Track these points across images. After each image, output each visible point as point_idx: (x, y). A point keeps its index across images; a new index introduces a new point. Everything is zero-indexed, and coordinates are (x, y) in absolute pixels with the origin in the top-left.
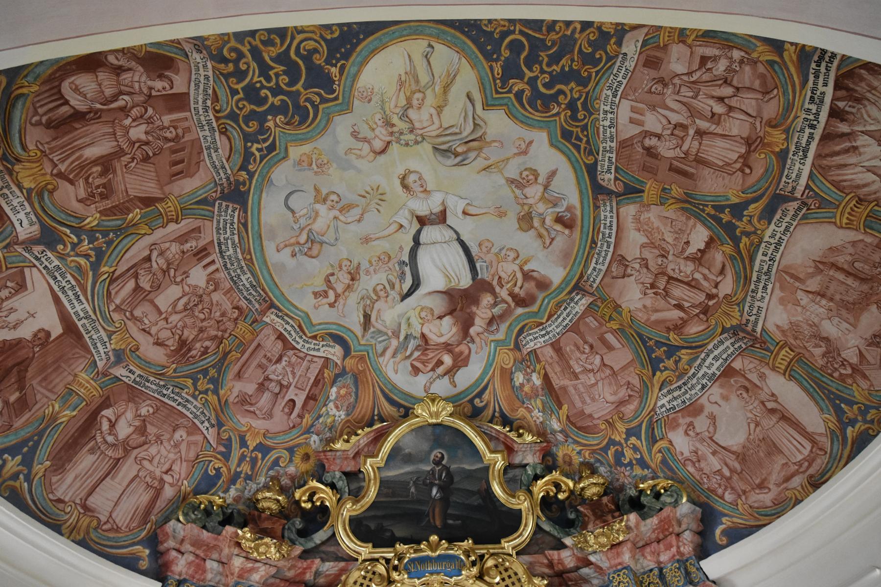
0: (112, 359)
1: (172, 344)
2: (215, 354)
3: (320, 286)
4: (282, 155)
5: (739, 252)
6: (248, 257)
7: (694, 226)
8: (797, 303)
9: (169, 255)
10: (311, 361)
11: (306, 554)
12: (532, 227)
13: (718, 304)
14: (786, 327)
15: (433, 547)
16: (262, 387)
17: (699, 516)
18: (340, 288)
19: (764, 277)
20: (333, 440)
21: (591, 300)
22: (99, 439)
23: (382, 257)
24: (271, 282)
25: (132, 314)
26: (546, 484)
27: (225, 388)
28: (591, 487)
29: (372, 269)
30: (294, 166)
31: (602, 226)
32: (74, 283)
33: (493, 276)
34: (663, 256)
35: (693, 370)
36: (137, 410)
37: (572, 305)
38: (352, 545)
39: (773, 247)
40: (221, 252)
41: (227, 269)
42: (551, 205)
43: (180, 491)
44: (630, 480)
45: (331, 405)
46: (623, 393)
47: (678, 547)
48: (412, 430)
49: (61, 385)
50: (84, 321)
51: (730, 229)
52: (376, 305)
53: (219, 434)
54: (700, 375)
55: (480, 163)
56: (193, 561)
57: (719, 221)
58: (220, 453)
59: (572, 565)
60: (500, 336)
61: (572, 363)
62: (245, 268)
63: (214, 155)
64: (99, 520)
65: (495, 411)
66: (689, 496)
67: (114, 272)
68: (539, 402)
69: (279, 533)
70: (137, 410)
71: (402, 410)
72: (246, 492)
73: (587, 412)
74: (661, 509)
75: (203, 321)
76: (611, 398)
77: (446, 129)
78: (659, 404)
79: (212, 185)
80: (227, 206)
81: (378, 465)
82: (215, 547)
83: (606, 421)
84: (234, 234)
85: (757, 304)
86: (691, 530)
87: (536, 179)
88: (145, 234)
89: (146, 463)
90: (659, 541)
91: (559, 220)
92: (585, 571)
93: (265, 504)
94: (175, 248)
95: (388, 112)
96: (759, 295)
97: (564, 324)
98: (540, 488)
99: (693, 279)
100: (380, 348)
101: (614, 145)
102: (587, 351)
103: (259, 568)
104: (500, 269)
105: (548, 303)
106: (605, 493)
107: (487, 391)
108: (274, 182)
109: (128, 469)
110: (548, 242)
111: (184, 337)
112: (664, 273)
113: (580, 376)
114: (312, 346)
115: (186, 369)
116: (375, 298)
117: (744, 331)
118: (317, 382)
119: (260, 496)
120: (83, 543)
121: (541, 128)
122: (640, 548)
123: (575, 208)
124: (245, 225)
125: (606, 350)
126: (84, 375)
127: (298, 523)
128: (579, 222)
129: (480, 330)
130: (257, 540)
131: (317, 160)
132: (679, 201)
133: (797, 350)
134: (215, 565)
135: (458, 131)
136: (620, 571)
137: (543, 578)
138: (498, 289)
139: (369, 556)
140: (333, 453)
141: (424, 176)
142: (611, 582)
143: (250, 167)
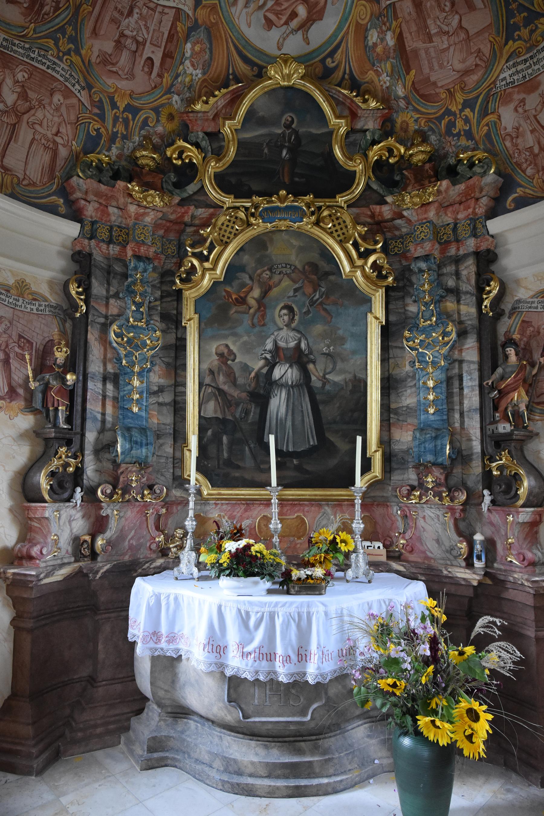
2: (67, 8)
10: (162, 13)
11: (183, 202)
15: (282, 200)
16: (119, 45)
17: (500, 185)
20: (192, 101)
26: (381, 149)
27: (86, 47)
36: (14, 77)
43: (72, 150)
44: (454, 149)
45: (187, 63)
46: (471, 61)
47: (474, 209)
48: (266, 93)
53: (90, 96)
56: (98, 208)
58: (96, 115)
59: (389, 217)
61: (429, 22)
64: (18, 178)
65: (345, 73)
66: (496, 168)
68: (388, 65)
69: (159, 185)
70: (14, 77)
71: (255, 68)
72: (125, 150)
73: (432, 79)
74: (471, 177)
76: (459, 66)
81: (236, 127)
82: (113, 197)
86: (489, 196)
89: (37, 127)
90: (460, 203)
92: (399, 222)
98: (374, 153)
102: (447, 9)
103: (149, 213)
106: (430, 160)
107: (340, 51)
113: (434, 39)
115: (44, 28)
118: (171, 37)
119: (138, 154)
120: (13, 196)
122: (444, 207)
127: (173, 177)
130: (144, 192)
134: (116, 210)
136: (424, 224)
137: (365, 225)
139: (232, 205)
140: (195, 115)
142: (415, 231)
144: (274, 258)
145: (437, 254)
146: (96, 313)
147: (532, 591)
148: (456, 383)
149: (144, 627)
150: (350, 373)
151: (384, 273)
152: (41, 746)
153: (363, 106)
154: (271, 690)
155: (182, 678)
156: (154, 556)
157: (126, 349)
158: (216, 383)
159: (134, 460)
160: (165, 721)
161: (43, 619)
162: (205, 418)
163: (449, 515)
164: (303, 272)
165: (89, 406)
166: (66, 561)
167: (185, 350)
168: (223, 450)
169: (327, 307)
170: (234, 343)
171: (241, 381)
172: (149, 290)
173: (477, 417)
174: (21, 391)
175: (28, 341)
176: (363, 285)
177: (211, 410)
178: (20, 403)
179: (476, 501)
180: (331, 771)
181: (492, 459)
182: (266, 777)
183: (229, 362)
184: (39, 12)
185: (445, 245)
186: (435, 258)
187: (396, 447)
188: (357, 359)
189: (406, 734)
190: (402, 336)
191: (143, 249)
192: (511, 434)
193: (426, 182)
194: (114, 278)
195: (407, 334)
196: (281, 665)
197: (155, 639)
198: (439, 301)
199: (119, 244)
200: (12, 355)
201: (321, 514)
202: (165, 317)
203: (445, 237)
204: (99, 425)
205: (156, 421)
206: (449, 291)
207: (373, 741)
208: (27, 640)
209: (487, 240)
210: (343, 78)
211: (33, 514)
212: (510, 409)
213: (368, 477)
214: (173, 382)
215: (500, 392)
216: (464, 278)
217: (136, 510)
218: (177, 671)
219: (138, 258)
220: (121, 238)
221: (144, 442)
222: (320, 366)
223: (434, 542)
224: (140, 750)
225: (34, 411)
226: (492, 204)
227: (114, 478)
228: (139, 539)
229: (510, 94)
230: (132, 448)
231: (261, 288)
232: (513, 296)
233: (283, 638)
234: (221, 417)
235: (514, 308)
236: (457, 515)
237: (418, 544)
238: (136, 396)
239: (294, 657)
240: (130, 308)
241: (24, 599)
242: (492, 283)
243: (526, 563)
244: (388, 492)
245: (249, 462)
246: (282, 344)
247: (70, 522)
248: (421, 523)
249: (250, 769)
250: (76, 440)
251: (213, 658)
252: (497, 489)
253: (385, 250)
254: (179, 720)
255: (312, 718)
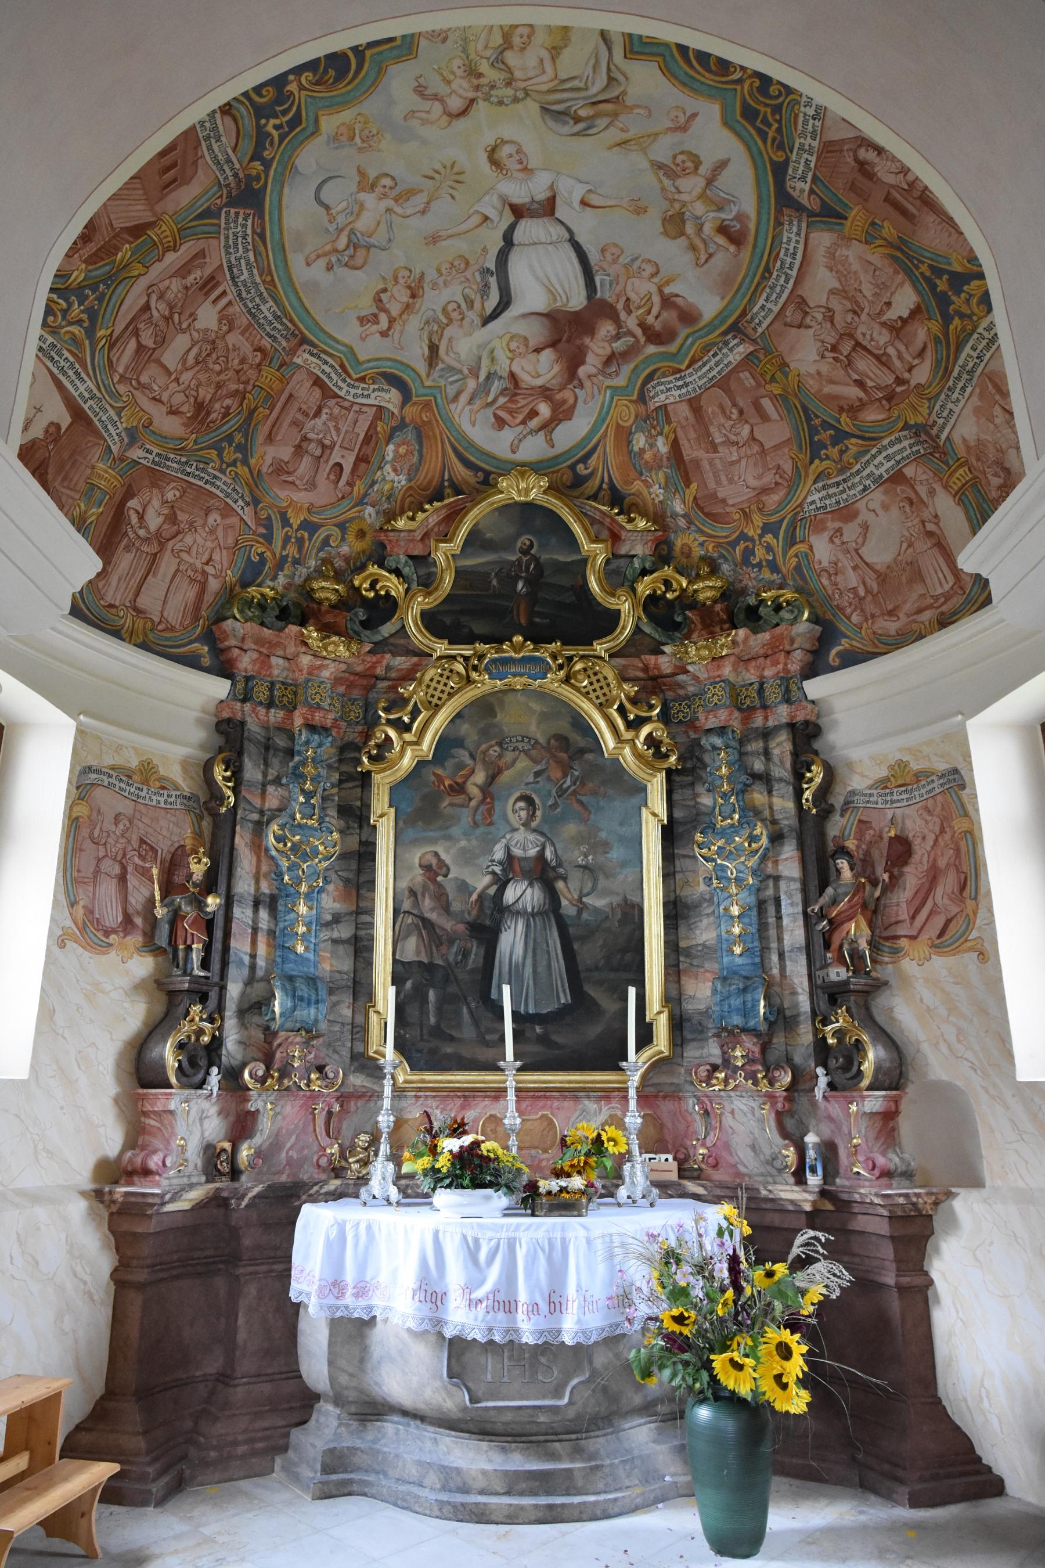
0: (126, 440)
1: (188, 409)
3: (367, 306)
4: (311, 129)
5: (946, 334)
6: (269, 279)
7: (901, 285)
8: (991, 419)
9: (170, 295)
12: (682, 233)
13: (906, 394)
14: (972, 444)
15: (516, 649)
16: (299, 450)
17: (818, 635)
18: (395, 309)
19: (965, 376)
20: (391, 516)
21: (752, 349)
22: (131, 535)
23: (456, 263)
24: (300, 310)
25: (139, 382)
27: (256, 456)
28: (706, 590)
29: (441, 281)
30: (328, 143)
31: (783, 251)
32: (72, 359)
33: (618, 296)
34: (855, 313)
35: (858, 466)
37: (725, 351)
38: (425, 641)
39: (984, 342)
40: (233, 278)
41: (242, 299)
42: (714, 208)
46: (769, 478)
47: (786, 664)
49: (82, 481)
50: (90, 402)
51: (943, 301)
52: (446, 332)
54: (865, 473)
55: (614, 135)
57: (933, 287)
59: (669, 671)
60: (621, 381)
61: (712, 429)
62: (265, 294)
63: (215, 147)
65: (602, 482)
67: (111, 335)
68: (661, 475)
73: (720, 495)
74: (778, 625)
75: (219, 373)
76: (753, 482)
77: (564, 81)
78: (810, 499)
79: (216, 188)
80: (237, 214)
82: (278, 644)
83: (742, 510)
84: (248, 251)
85: (950, 405)
87: (696, 168)
88: (140, 275)
89: (184, 556)
90: (766, 657)
91: (723, 230)
92: (682, 678)
93: (322, 595)
94: (176, 285)
95: (473, 56)
96: (955, 395)
97: (710, 376)
99: (885, 354)
100: (451, 391)
101: (815, 144)
102: (734, 417)
104: (629, 288)
105: (693, 343)
107: (595, 455)
108: (300, 169)
109: (167, 565)
110: (703, 257)
111: (200, 399)
112: (851, 336)
113: (720, 449)
114: (360, 392)
115: (207, 437)
116: (445, 321)
117: (928, 434)
118: (367, 439)
120: (144, 646)
121: (710, 97)
122: (744, 661)
123: (748, 217)
124: (262, 237)
125: (759, 420)
126: (100, 465)
127: (362, 614)
128: (751, 239)
129: (594, 371)
131: (362, 131)
132: (890, 245)
133: (976, 473)
134: (281, 661)
135: (582, 85)
138: (623, 315)
141: (525, 149)
143: (266, 153)
144: (505, 729)
145: (736, 725)
146: (248, 807)
147: (885, 1213)
148: (771, 910)
149: (322, 1271)
150: (618, 894)
151: (664, 750)
152: (158, 1466)
153: (629, 527)
154: (510, 1358)
155: (376, 1351)
156: (323, 1177)
157: (289, 859)
158: (420, 910)
159: (298, 1025)
160: (348, 1425)
161: (161, 1270)
162: (403, 963)
163: (767, 1107)
164: (548, 748)
165: (233, 944)
166: (194, 1180)
167: (374, 860)
168: (428, 1013)
169: (584, 799)
170: (447, 851)
171: (456, 906)
172: (323, 772)
173: (803, 960)
174: (138, 921)
175: (152, 848)
176: (634, 767)
177: (411, 949)
178: (136, 939)
179: (807, 1086)
180: (601, 1486)
181: (825, 1022)
182: (504, 1494)
183: (440, 879)
184: (202, 422)
185: (747, 712)
186: (733, 731)
187: (690, 1007)
188: (627, 875)
189: (703, 1401)
190: (693, 842)
191: (318, 716)
192: (846, 983)
193: (718, 629)
194: (274, 755)
195: (698, 837)
196: (525, 1317)
197: (335, 1291)
198: (743, 792)
199: (283, 707)
200: (130, 869)
201: (578, 1113)
202: (344, 811)
203: (748, 702)
204: (246, 972)
205: (328, 968)
206: (756, 777)
207: (663, 1448)
208: (135, 1301)
209: (805, 708)
210: (600, 488)
211: (152, 1105)
212: (846, 947)
213: (648, 1053)
214: (354, 908)
215: (831, 922)
216: (776, 759)
217: (299, 1103)
218: (368, 1342)
219: (312, 728)
220: (285, 699)
221: (313, 998)
222: (574, 884)
223: (749, 1150)
224: (310, 1473)
225: (156, 951)
226: (809, 658)
227: (265, 1055)
228: (303, 1148)
229: (822, 521)
230: (294, 1008)
231: (487, 771)
232: (845, 785)
233: (528, 1275)
234: (426, 961)
235: (847, 803)
236: (779, 1106)
237: (724, 1154)
238: (302, 929)
239: (544, 1307)
240: (296, 800)
241: (135, 1235)
242: (814, 768)
243: (877, 1172)
244: (680, 1076)
245: (468, 1031)
246: (517, 852)
247: (201, 1120)
248: (728, 1120)
249: (481, 1483)
250: (213, 995)
251: (426, 1310)
252: (832, 1063)
253: (665, 717)
254: (369, 1424)
255: (571, 1403)
